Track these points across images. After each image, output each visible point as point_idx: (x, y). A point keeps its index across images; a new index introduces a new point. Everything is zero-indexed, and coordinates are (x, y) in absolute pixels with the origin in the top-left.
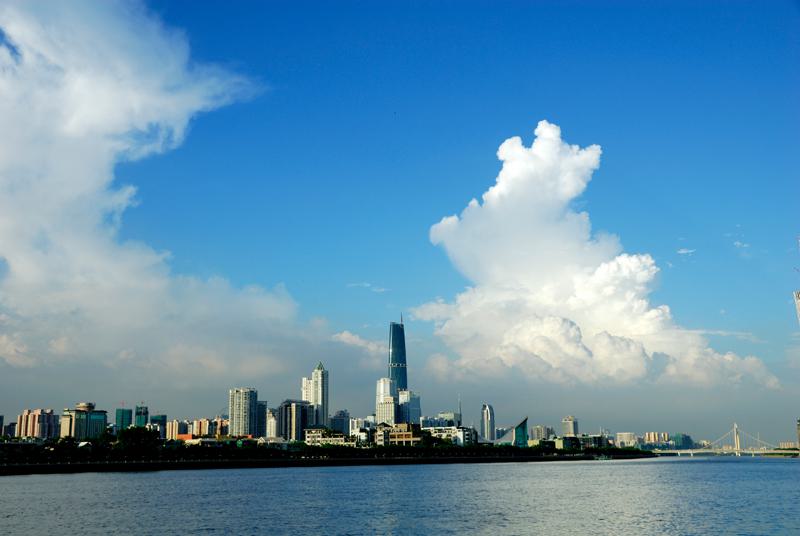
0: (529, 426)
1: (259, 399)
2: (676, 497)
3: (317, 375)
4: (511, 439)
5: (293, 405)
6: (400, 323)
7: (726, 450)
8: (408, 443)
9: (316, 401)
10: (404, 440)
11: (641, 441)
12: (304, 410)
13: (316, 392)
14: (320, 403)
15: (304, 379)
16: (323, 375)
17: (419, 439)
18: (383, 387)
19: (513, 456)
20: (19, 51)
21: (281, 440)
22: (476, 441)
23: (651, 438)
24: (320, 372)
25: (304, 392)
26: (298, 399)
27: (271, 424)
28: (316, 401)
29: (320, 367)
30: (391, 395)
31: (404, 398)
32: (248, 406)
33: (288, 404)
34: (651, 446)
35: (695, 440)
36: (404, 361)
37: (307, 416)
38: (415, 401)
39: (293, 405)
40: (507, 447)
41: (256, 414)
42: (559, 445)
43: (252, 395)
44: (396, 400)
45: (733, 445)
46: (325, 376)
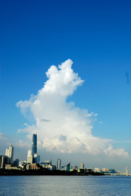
4: (65, 169)
5: (3, 157)
6: (36, 134)
7: (124, 174)
8: (33, 169)
9: (10, 156)
10: (35, 168)
11: (101, 170)
13: (10, 153)
14: (11, 156)
15: (7, 149)
16: (12, 148)
17: (39, 168)
18: (30, 153)
23: (104, 170)
24: (11, 147)
25: (6, 153)
26: (4, 155)
29: (12, 146)
30: (32, 155)
31: (35, 156)
34: (104, 172)
35: (116, 171)
38: (39, 157)
39: (3, 157)
42: (79, 171)
44: (33, 156)
46: (13, 149)
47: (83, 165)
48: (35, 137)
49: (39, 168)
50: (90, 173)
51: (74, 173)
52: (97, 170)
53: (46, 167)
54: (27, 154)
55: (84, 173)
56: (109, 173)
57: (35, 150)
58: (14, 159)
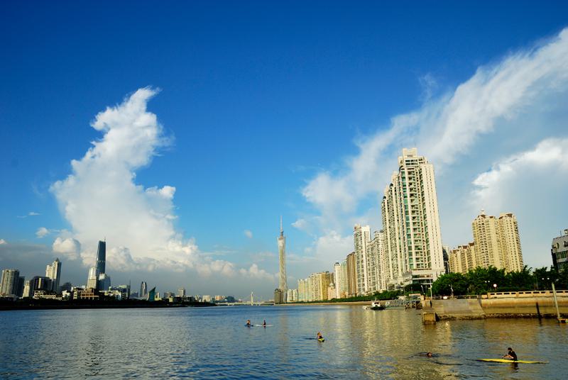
0: (156, 291)
1: (20, 275)
2: (58, 323)
3: (55, 264)
4: (147, 297)
5: (40, 279)
6: (103, 241)
7: (248, 303)
8: (91, 298)
9: (53, 277)
11: (213, 299)
12: (46, 282)
13: (54, 272)
14: (55, 278)
16: (58, 264)
17: (553, 285)
18: (92, 274)
19: (39, 305)
20: (536, 53)
21: (13, 296)
23: (218, 298)
24: (57, 263)
25: (47, 273)
26: (42, 276)
27: (27, 289)
29: (57, 260)
31: (102, 277)
32: (13, 279)
33: (37, 279)
34: (217, 302)
35: (235, 298)
37: (47, 285)
38: (107, 279)
39: (40, 279)
40: (144, 301)
41: (18, 283)
42: (171, 300)
43: (16, 273)
44: (97, 278)
45: (250, 300)
46: (59, 265)
47: (184, 291)
48: (102, 246)
49: (553, 285)
50: (192, 303)
51: (164, 304)
52: (207, 298)
54: (87, 275)
55: (181, 302)
56: (225, 302)
57: (101, 267)
58: (62, 283)
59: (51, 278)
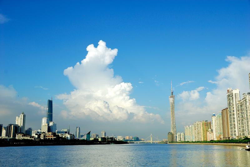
9: (21, 124)
12: (16, 128)
13: (21, 122)
15: (17, 117)
18: (44, 121)
21: (7, 137)
22: (74, 138)
28: (21, 124)
30: (47, 123)
36: (52, 112)
44: (48, 125)
46: (24, 116)
53: (64, 136)
59: (19, 125)
